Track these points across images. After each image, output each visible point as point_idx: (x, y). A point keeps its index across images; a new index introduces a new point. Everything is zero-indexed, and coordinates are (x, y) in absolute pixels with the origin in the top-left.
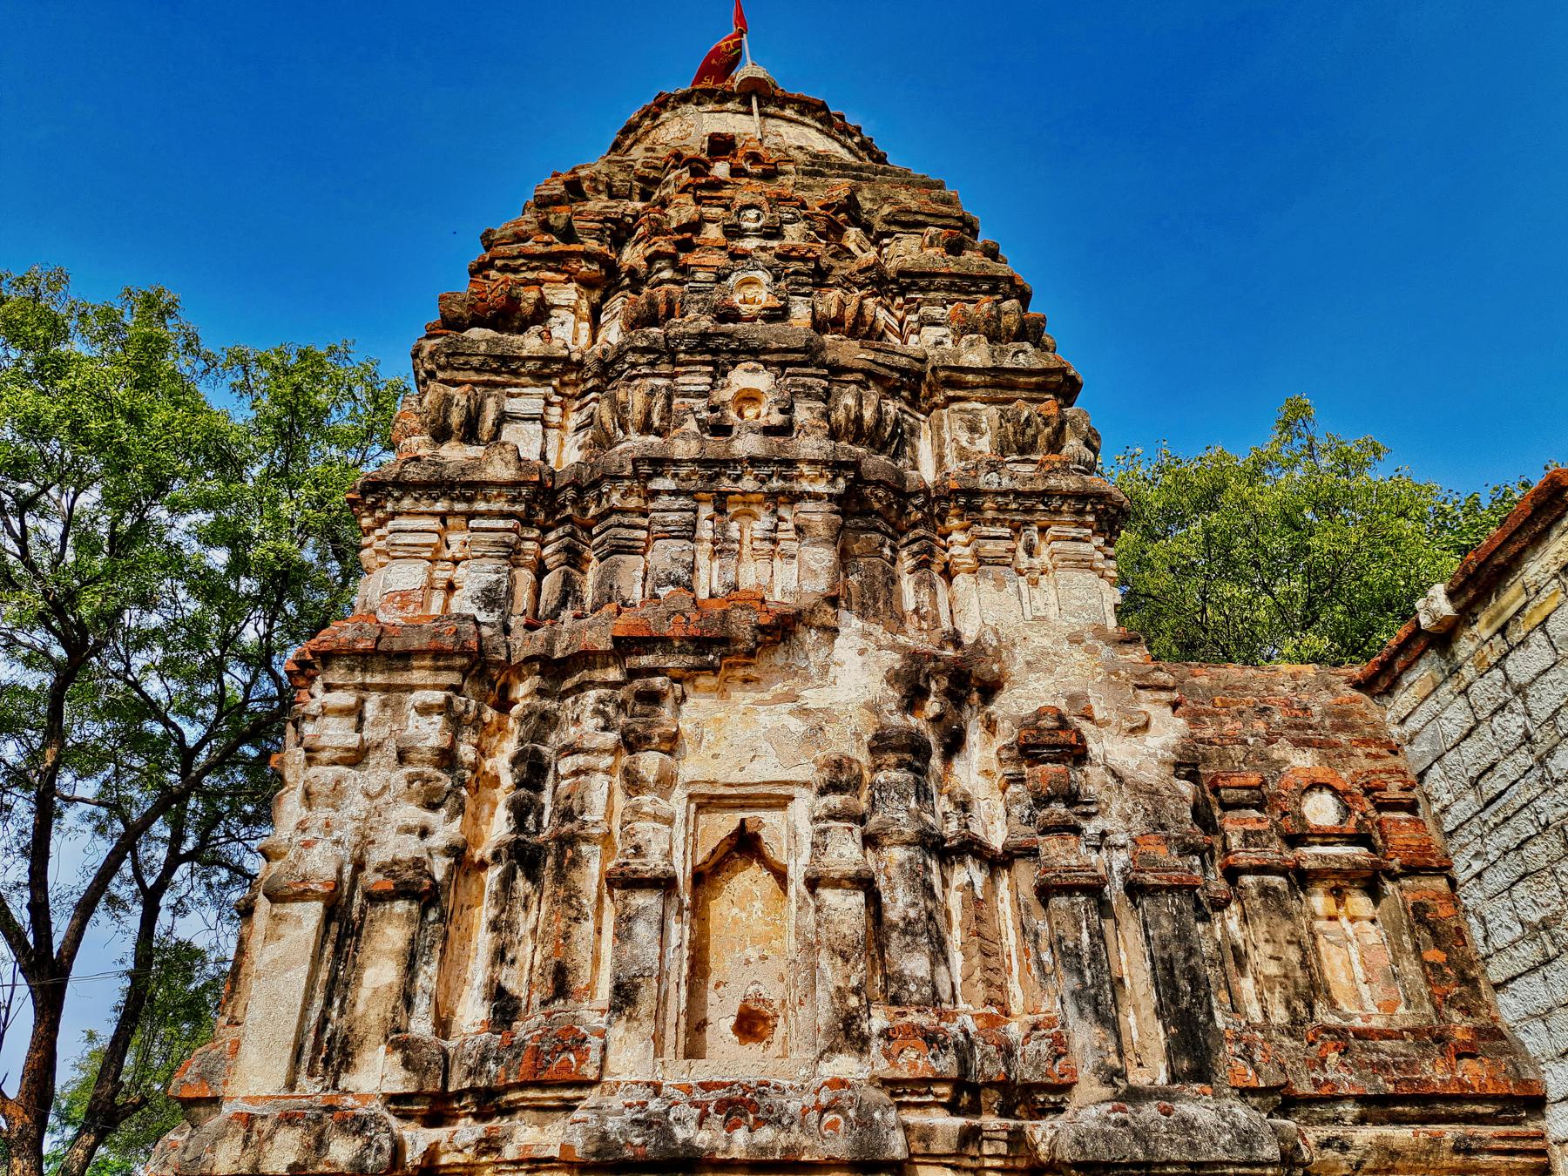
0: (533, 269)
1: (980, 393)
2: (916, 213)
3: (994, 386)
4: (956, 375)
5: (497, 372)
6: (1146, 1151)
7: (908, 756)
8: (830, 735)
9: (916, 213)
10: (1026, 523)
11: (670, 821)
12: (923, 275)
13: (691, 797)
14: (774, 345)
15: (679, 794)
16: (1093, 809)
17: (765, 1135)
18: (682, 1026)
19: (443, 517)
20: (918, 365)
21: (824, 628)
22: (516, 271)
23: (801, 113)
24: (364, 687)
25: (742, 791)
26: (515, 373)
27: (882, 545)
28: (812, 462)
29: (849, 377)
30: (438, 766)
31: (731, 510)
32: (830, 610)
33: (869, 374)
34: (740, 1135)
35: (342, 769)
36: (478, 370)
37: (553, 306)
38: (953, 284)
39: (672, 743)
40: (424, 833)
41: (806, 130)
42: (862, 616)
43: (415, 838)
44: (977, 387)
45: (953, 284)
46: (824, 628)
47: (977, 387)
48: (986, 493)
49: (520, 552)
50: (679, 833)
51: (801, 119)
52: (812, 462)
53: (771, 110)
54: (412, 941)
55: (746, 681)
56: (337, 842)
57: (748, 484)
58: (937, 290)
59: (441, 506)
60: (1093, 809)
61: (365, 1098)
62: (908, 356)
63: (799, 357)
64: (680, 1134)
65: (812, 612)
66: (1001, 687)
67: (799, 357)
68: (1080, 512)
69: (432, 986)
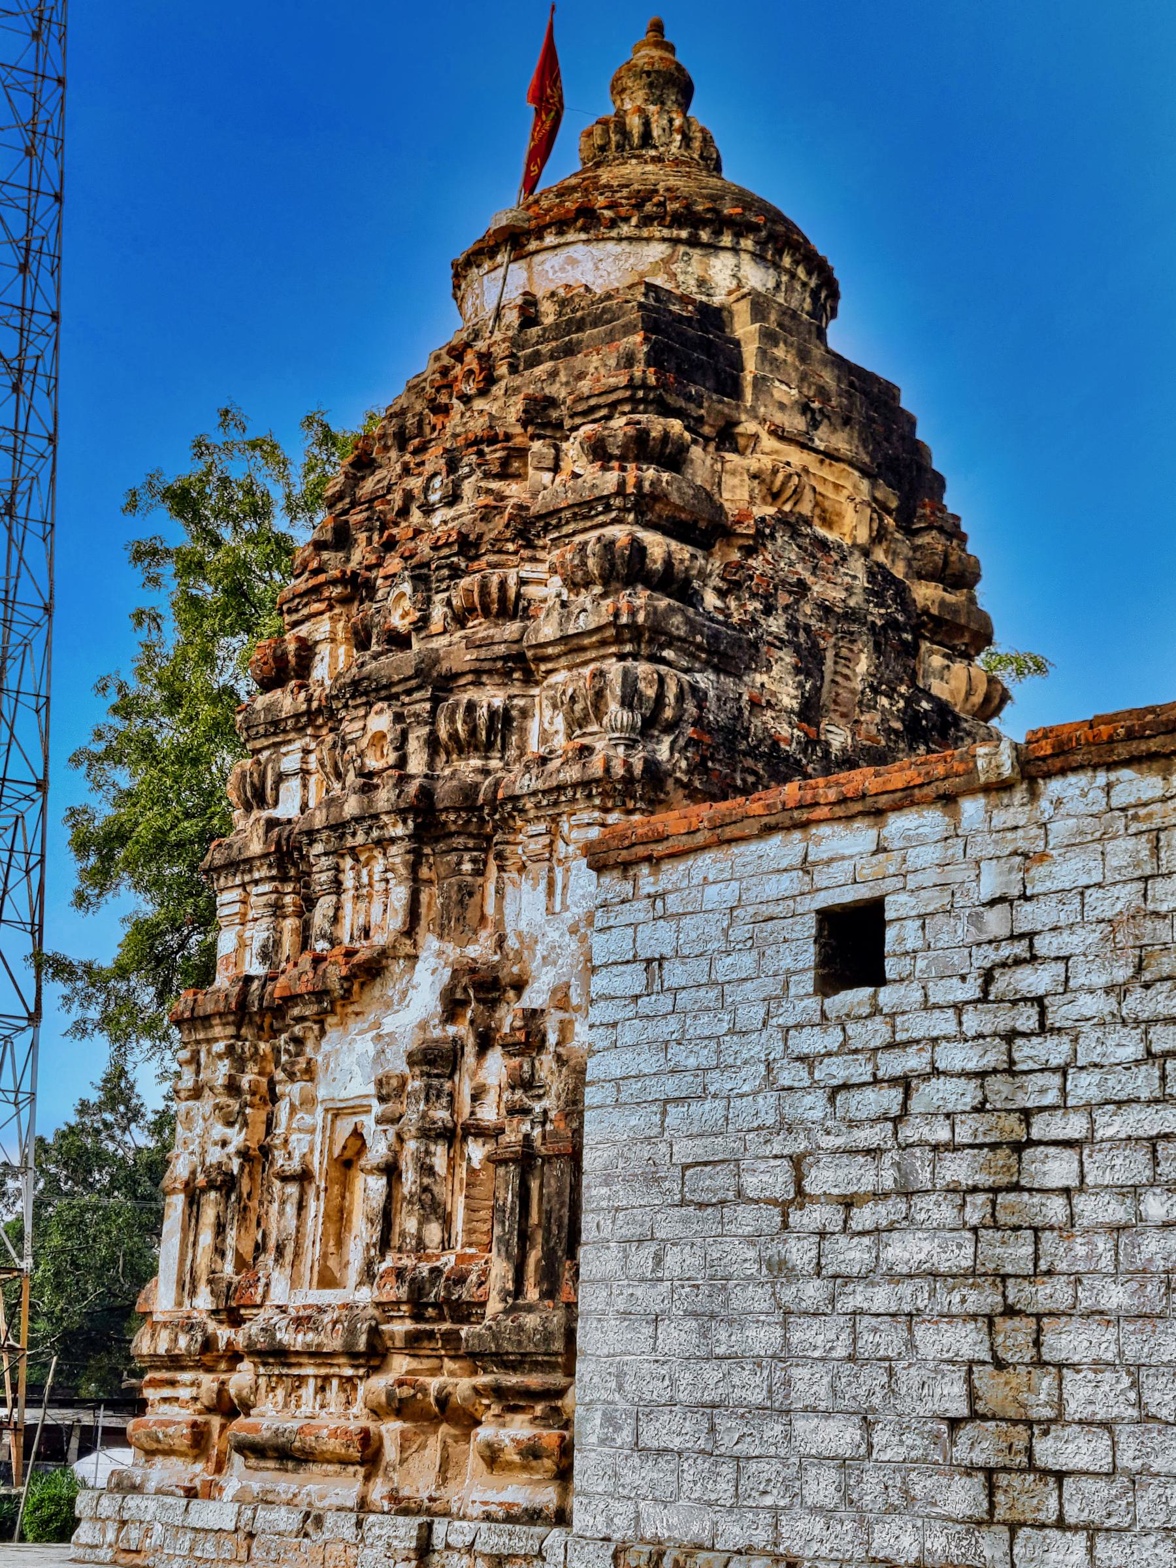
0: (305, 605)
1: (563, 662)
2: (589, 397)
3: (571, 651)
4: (540, 651)
5: (275, 734)
6: (497, 1345)
7: (425, 1068)
8: (389, 1056)
9: (589, 397)
10: (559, 815)
11: (312, 1131)
12: (551, 514)
13: (327, 1110)
14: (396, 678)
15: (320, 1109)
16: (541, 1091)
17: (311, 1336)
18: (316, 1269)
19: (243, 885)
20: (516, 647)
21: (408, 957)
22: (297, 611)
23: (561, 233)
24: (198, 1042)
25: (351, 1103)
26: (285, 731)
27: (459, 863)
28: (387, 813)
29: (463, 681)
30: (230, 1096)
31: (363, 858)
32: (408, 942)
33: (478, 672)
34: (300, 1337)
35: (190, 1103)
36: (265, 736)
37: (317, 643)
38: (575, 514)
39: (309, 1072)
40: (224, 1144)
41: (571, 249)
42: (441, 937)
43: (219, 1148)
44: (559, 656)
45: (575, 514)
46: (408, 957)
47: (559, 656)
48: (522, 796)
49: (283, 906)
50: (318, 1138)
51: (562, 240)
52: (387, 813)
53: (533, 245)
54: (218, 1217)
55: (357, 1014)
56: (192, 1153)
57: (360, 838)
58: (567, 523)
59: (238, 881)
60: (541, 1091)
61: (200, 1312)
62: (505, 642)
63: (413, 683)
64: (279, 1336)
65: (394, 947)
66: (526, 982)
67: (413, 683)
68: (589, 797)
69: (233, 1243)
